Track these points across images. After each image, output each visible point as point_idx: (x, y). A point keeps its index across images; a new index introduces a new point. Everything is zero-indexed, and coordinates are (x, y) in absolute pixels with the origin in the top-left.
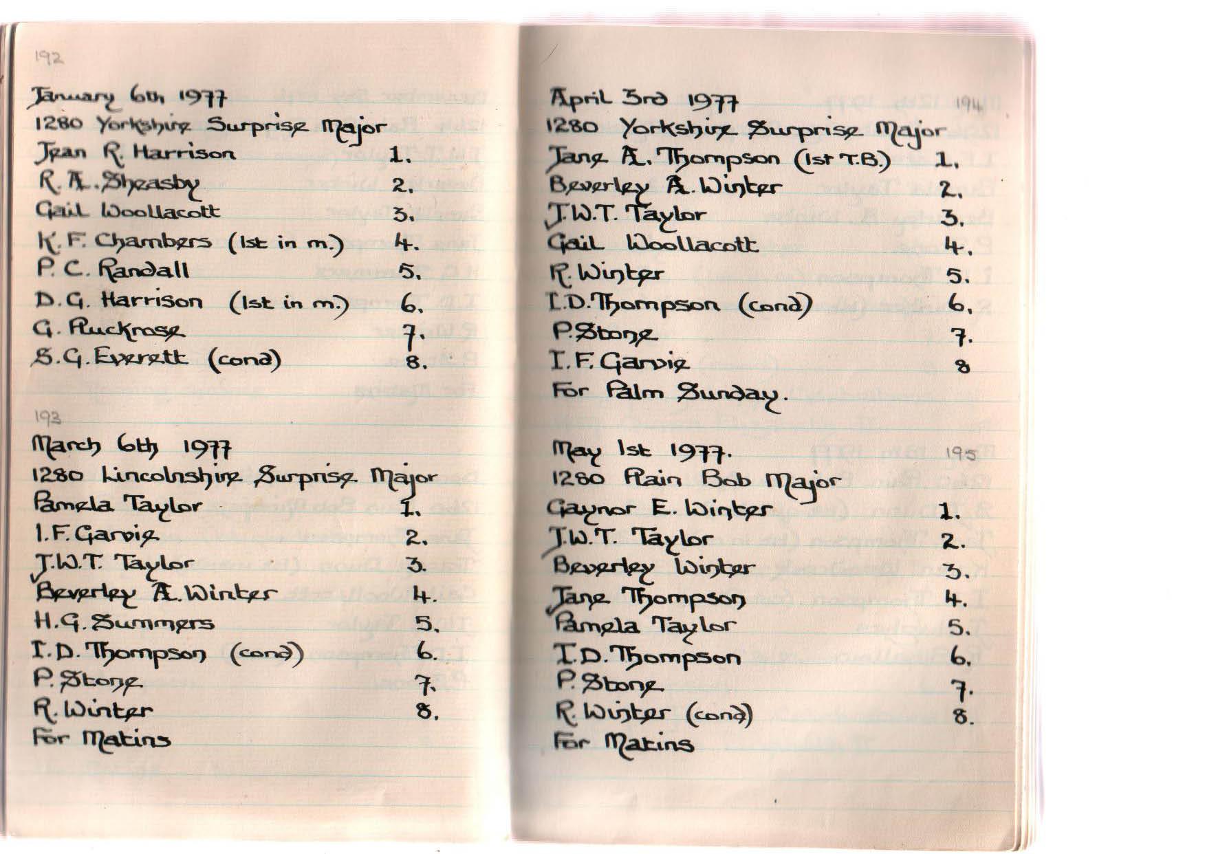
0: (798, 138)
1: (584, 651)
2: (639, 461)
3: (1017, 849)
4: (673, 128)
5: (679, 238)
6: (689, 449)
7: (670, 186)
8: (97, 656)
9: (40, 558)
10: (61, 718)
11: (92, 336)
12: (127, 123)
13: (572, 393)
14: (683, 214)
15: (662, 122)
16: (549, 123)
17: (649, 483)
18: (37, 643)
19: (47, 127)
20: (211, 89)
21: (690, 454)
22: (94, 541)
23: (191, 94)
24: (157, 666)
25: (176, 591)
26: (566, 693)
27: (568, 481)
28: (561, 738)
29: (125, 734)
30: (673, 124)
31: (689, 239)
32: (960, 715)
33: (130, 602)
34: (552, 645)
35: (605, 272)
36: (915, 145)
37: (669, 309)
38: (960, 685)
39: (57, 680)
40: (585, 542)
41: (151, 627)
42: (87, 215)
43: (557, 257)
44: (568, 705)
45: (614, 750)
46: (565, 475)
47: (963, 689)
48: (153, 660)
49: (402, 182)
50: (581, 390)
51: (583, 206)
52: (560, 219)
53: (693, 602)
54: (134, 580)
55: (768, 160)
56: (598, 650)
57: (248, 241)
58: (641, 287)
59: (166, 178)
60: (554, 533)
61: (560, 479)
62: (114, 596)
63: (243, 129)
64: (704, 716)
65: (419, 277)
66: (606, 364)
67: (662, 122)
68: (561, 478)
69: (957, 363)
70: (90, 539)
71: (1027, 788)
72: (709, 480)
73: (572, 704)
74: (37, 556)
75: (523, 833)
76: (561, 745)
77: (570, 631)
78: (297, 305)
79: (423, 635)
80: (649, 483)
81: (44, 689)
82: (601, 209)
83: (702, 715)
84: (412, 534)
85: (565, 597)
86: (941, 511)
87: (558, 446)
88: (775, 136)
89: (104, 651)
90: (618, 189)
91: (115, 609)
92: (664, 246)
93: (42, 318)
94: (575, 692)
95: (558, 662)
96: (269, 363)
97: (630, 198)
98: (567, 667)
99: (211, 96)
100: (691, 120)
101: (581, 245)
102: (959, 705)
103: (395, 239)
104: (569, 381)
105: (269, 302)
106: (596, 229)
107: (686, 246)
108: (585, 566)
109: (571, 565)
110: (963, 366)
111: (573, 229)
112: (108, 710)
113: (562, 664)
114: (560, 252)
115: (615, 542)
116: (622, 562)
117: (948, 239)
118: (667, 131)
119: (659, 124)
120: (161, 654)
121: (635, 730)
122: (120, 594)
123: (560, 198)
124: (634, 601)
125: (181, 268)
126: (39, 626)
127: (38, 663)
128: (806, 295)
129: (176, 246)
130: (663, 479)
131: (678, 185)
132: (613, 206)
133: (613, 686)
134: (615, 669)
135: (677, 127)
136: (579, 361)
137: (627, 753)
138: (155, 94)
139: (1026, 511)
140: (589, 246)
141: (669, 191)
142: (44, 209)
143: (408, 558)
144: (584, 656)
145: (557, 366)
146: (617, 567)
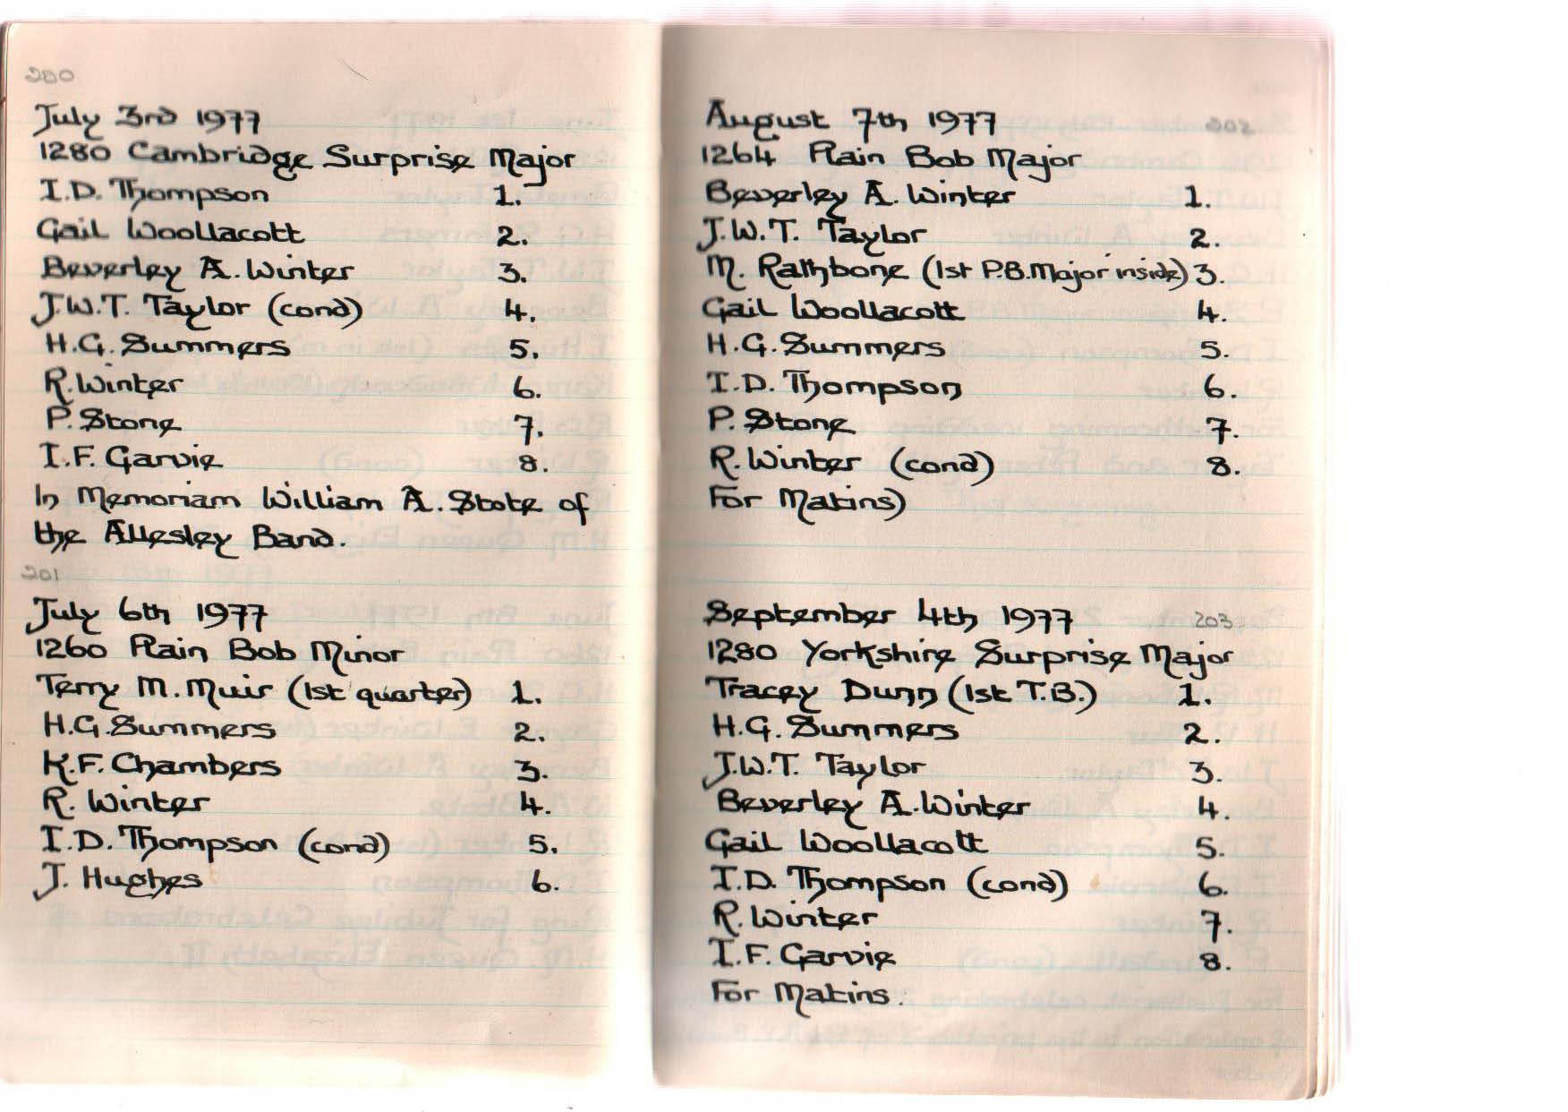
0: (1042, 666)
1: (749, 873)
2: (155, 627)
3: (1312, 1094)
4: (874, 654)
9: (45, 448)
11: (151, 677)
12: (809, 800)
13: (734, 503)
15: (857, 644)
16: (704, 151)
17: (843, 161)
19: (715, 161)
20: (969, 111)
21: (953, 123)
22: (133, 469)
24: (211, 860)
26: (722, 436)
28: (722, 987)
30: (874, 647)
34: (707, 940)
36: (1199, 674)
37: (207, 199)
38: (1212, 917)
42: (106, 237)
43: (715, 326)
44: (727, 452)
45: (792, 509)
49: (510, 231)
50: (748, 499)
51: (755, 759)
52: (727, 771)
55: (262, 846)
56: (773, 285)
58: (832, 441)
63: (898, 696)
65: (555, 850)
67: (857, 644)
68: (717, 155)
69: (1202, 957)
72: (918, 160)
73: (732, 450)
74: (43, 182)
76: (722, 997)
77: (736, 316)
80: (843, 161)
82: (779, 760)
86: (498, 195)
87: (718, 610)
88: (182, 468)
89: (142, 838)
90: (817, 807)
92: (853, 847)
93: (49, 216)
94: (737, 436)
96: (375, 850)
99: (238, 118)
100: (933, 626)
102: (1210, 948)
103: (504, 306)
104: (735, 979)
105: (822, 117)
108: (755, 192)
109: (732, 193)
112: (804, 461)
114: (721, 853)
117: (508, 302)
118: (864, 657)
119: (854, 648)
121: (817, 484)
122: (162, 271)
123: (52, 285)
124: (802, 887)
126: (51, 349)
128: (1175, 677)
129: (733, 201)
130: (182, 650)
132: (794, 221)
133: (116, 424)
134: (790, 404)
135: (880, 652)
137: (807, 513)
138: (891, 116)
139: (1321, 758)
146: (128, 270)
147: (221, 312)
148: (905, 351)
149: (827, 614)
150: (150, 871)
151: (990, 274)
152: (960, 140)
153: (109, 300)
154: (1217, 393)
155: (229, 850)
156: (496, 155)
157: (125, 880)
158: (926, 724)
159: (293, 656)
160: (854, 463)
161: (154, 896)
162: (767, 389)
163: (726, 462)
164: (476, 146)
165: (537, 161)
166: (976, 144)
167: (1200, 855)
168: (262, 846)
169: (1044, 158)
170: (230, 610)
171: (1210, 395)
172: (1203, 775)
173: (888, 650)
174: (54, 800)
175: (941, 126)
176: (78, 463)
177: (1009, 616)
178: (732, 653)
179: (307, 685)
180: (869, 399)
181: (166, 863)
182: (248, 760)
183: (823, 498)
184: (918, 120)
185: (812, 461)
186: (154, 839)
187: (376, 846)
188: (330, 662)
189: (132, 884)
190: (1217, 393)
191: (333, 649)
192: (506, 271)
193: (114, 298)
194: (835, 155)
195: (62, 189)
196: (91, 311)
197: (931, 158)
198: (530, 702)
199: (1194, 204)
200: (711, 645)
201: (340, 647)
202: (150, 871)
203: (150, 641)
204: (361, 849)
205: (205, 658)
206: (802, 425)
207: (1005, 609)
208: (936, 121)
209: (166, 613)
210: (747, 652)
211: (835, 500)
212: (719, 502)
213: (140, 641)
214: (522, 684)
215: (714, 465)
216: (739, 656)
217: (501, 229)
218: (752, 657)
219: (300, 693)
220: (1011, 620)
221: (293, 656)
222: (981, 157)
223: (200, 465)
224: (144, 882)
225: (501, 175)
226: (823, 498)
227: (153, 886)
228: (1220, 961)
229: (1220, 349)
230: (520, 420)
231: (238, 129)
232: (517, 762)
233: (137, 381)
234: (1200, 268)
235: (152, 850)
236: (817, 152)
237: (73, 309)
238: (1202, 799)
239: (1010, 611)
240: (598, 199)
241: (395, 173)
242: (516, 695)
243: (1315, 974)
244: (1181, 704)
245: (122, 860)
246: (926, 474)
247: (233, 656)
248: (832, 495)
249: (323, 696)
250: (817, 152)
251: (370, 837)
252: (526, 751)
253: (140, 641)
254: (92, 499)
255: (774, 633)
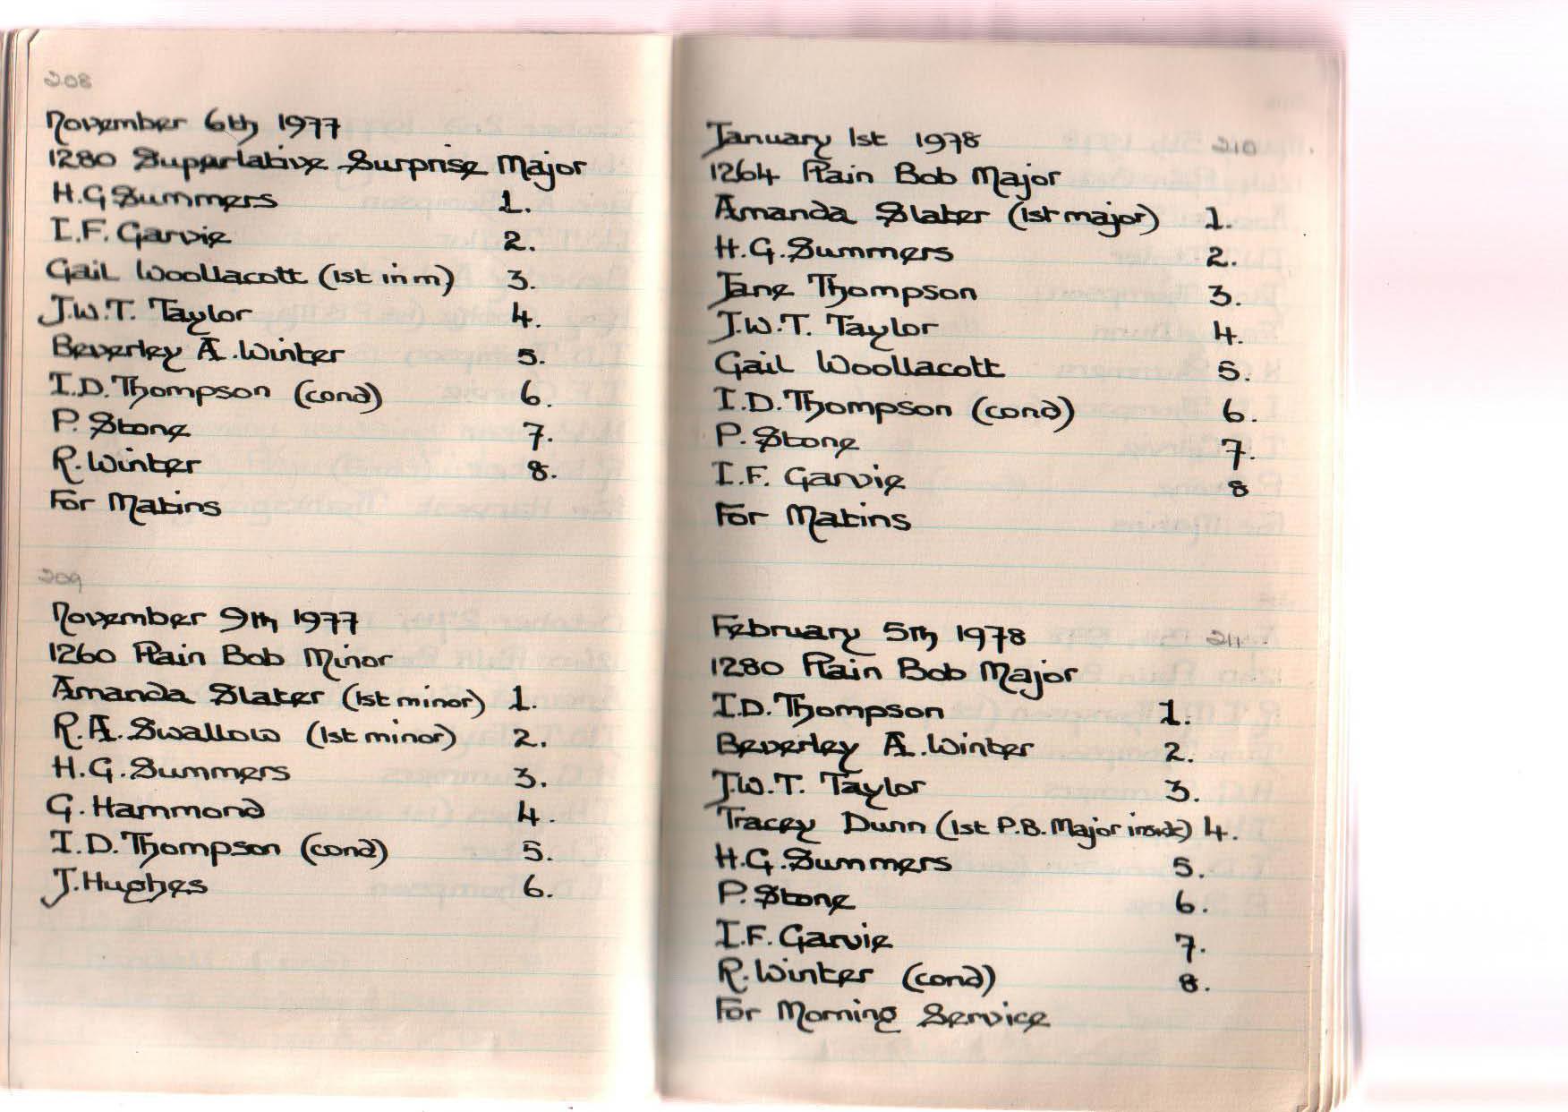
5: (894, 358)
6: (936, 139)
7: (888, 746)
8: (126, 393)
10: (86, 473)
14: (898, 786)
18: (58, 377)
20: (317, 117)
23: (292, 121)
25: (227, 346)
27: (731, 670)
28: (725, 1005)
29: (155, 458)
31: (906, 360)
32: (1189, 983)
33: (173, 363)
35: (791, 973)
39: (85, 425)
40: (761, 792)
41: (207, 777)
44: (69, 452)
45: (801, 527)
46: (727, 663)
47: (1238, 452)
48: (210, 857)
52: (731, 333)
53: (215, 853)
54: (174, 335)
55: (265, 850)
57: (343, 274)
59: (280, 765)
60: (720, 778)
61: (719, 173)
62: (154, 354)
64: (928, 981)
66: (792, 479)
70: (806, 484)
71: (1330, 1031)
73: (74, 451)
75: (666, 1087)
78: (399, 279)
79: (533, 867)
81: (66, 436)
83: (925, 979)
84: (1216, 252)
85: (725, 136)
91: (150, 373)
95: (718, 943)
96: (371, 855)
97: (831, 763)
98: (731, 953)
101: (764, 367)
106: (781, 343)
107: (902, 369)
110: (1189, 983)
111: (749, 346)
113: (721, 947)
115: (802, 792)
116: (811, 405)
120: (220, 848)
125: (803, 405)
127: (62, 861)
131: (899, 745)
136: (750, 477)
140: (775, 367)
141: (886, 752)
142: (59, 269)
143: (517, 769)
144: (752, 404)
145: (726, 406)
147: (906, 333)
148: (322, 358)
149: (135, 618)
150: (149, 876)
151: (811, 405)
152: (949, 160)
153: (114, 306)
154: (1237, 417)
155: (233, 855)
156: (980, 173)
157: (124, 887)
158: (797, 741)
159: (963, 674)
160: (194, 466)
161: (151, 901)
162: (775, 409)
163: (66, 462)
164: (483, 152)
165: (1021, 180)
166: (959, 163)
167: (1178, 874)
168: (265, 850)
169: (1025, 177)
170: (340, 617)
171: (1230, 420)
172: (527, 781)
173: (371, 696)
174: (64, 728)
175: (290, 130)
176: (751, 481)
177: (962, 634)
178: (738, 668)
179: (358, 693)
180: (865, 417)
181: (164, 869)
182: (242, 194)
183: (152, 502)
184: (268, 122)
185: (151, 464)
186: (155, 846)
187: (373, 849)
188: (321, 668)
189: (130, 889)
190: (1237, 417)
191: (324, 656)
192: (1175, 789)
193: (120, 304)
194: (825, 175)
195: (72, 384)
196: (96, 317)
197: (916, 176)
198: (519, 211)
199: (1216, 226)
200: (714, 662)
201: (330, 654)
202: (149, 876)
203: (154, 649)
204: (358, 853)
205: (879, 676)
206: (141, 429)
207: (959, 628)
208: (286, 126)
209: (274, 623)
210: (753, 667)
211: (846, 516)
212: (725, 519)
213: (143, 649)
214: (1174, 704)
215: (56, 467)
216: (746, 670)
217: (1212, 249)
218: (757, 672)
219: (352, 699)
220: (965, 638)
221: (282, 661)
222: (965, 176)
223: (900, 258)
224: (143, 888)
225: (514, 180)
226: (152, 502)
227: (151, 889)
228: (1197, 983)
229: (1238, 369)
230: (1228, 443)
231: (318, 135)
232: (1168, 782)
233: (152, 462)
234: (512, 274)
235: (152, 856)
236: (729, 894)
237: (80, 315)
238: (522, 804)
239: (964, 629)
240: (618, 210)
241: (414, 178)
242: (515, 702)
243: (1318, 991)
244: (1162, 722)
245: (125, 864)
246: (104, 473)
247: (227, 662)
248: (161, 500)
249: (227, 395)
250: (729, 894)
251: (366, 841)
252: (525, 756)
253: (143, 649)
254: (986, 181)
255: (760, 649)
